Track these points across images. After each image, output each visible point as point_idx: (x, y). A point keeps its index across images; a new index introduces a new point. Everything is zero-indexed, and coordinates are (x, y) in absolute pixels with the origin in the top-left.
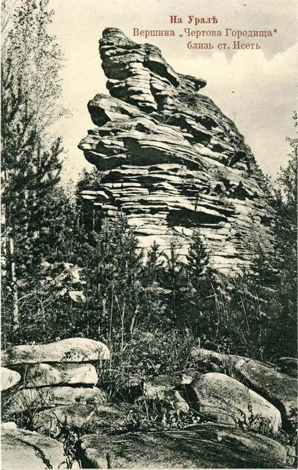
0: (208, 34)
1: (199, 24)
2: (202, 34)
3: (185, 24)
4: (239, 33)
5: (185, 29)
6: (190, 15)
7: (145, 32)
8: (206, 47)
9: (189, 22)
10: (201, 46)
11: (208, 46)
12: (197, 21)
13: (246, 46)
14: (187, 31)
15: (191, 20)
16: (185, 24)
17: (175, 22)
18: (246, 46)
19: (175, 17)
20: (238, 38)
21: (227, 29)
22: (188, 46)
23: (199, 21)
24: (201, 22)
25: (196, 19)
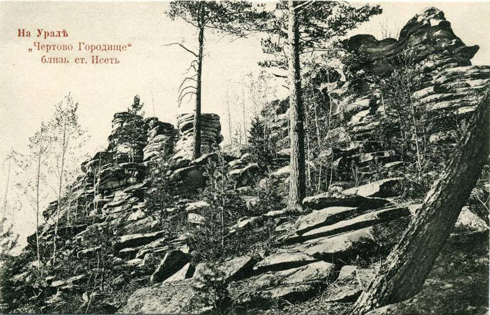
0: (59, 48)
1: (49, 38)
2: (52, 48)
3: (34, 38)
4: (92, 48)
5: (35, 43)
6: (40, 29)
7: (46, 46)
8: (61, 61)
9: (38, 36)
10: (55, 60)
11: (64, 60)
12: (47, 34)
13: (105, 61)
14: (37, 44)
15: (40, 33)
16: (34, 38)
17: (23, 36)
18: (105, 61)
19: (23, 30)
20: (92, 52)
21: (80, 43)
22: (76, 61)
23: (48, 35)
24: (51, 36)
25: (45, 32)
